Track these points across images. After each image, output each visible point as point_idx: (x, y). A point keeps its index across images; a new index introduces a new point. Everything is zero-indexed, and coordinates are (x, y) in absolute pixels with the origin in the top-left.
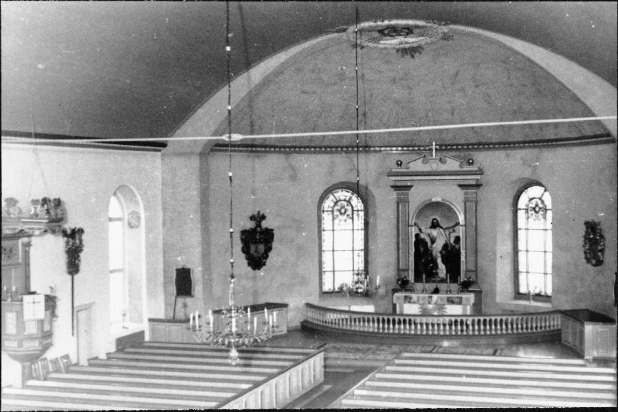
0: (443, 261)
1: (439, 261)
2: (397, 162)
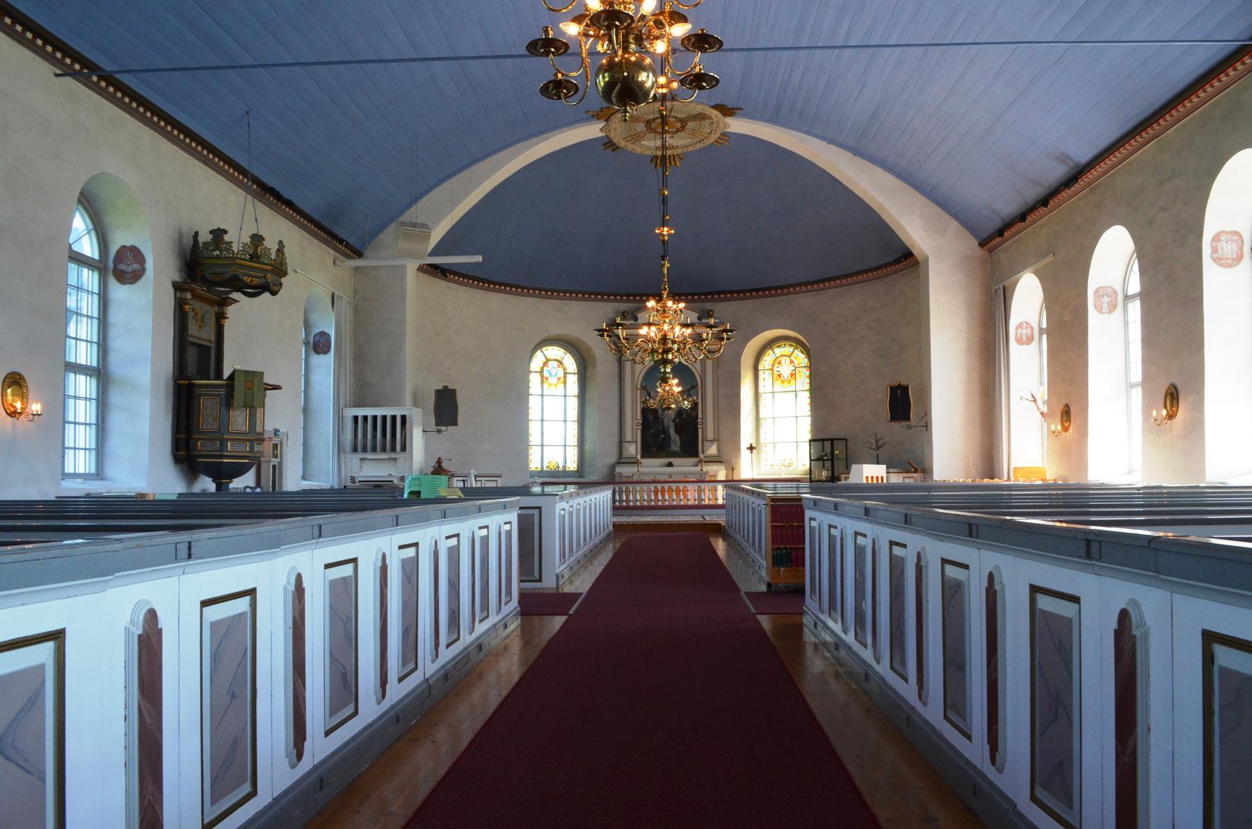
0: (676, 432)
1: (672, 431)
2: (713, 311)
